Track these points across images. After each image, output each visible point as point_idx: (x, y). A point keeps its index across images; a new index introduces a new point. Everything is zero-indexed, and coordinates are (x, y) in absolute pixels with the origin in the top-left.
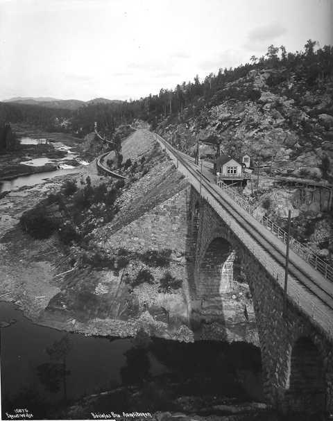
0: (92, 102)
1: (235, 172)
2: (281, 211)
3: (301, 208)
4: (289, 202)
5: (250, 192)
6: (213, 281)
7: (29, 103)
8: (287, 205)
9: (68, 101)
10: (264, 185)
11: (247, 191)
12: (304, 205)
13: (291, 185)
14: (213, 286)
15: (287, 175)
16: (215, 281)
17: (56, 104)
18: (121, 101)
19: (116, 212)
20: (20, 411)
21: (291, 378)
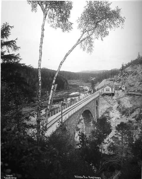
0: (111, 70)
1: (109, 90)
2: (125, 105)
3: (134, 104)
4: (129, 102)
5: (115, 98)
6: (88, 128)
7: (87, 72)
8: (128, 103)
9: (67, 72)
10: (121, 96)
11: (114, 97)
12: (135, 103)
13: (130, 95)
14: (88, 130)
15: (133, 92)
16: (89, 128)
17: (97, 72)
18: (107, 70)
19: (83, 113)
20: (9, 176)
21: (38, 77)
